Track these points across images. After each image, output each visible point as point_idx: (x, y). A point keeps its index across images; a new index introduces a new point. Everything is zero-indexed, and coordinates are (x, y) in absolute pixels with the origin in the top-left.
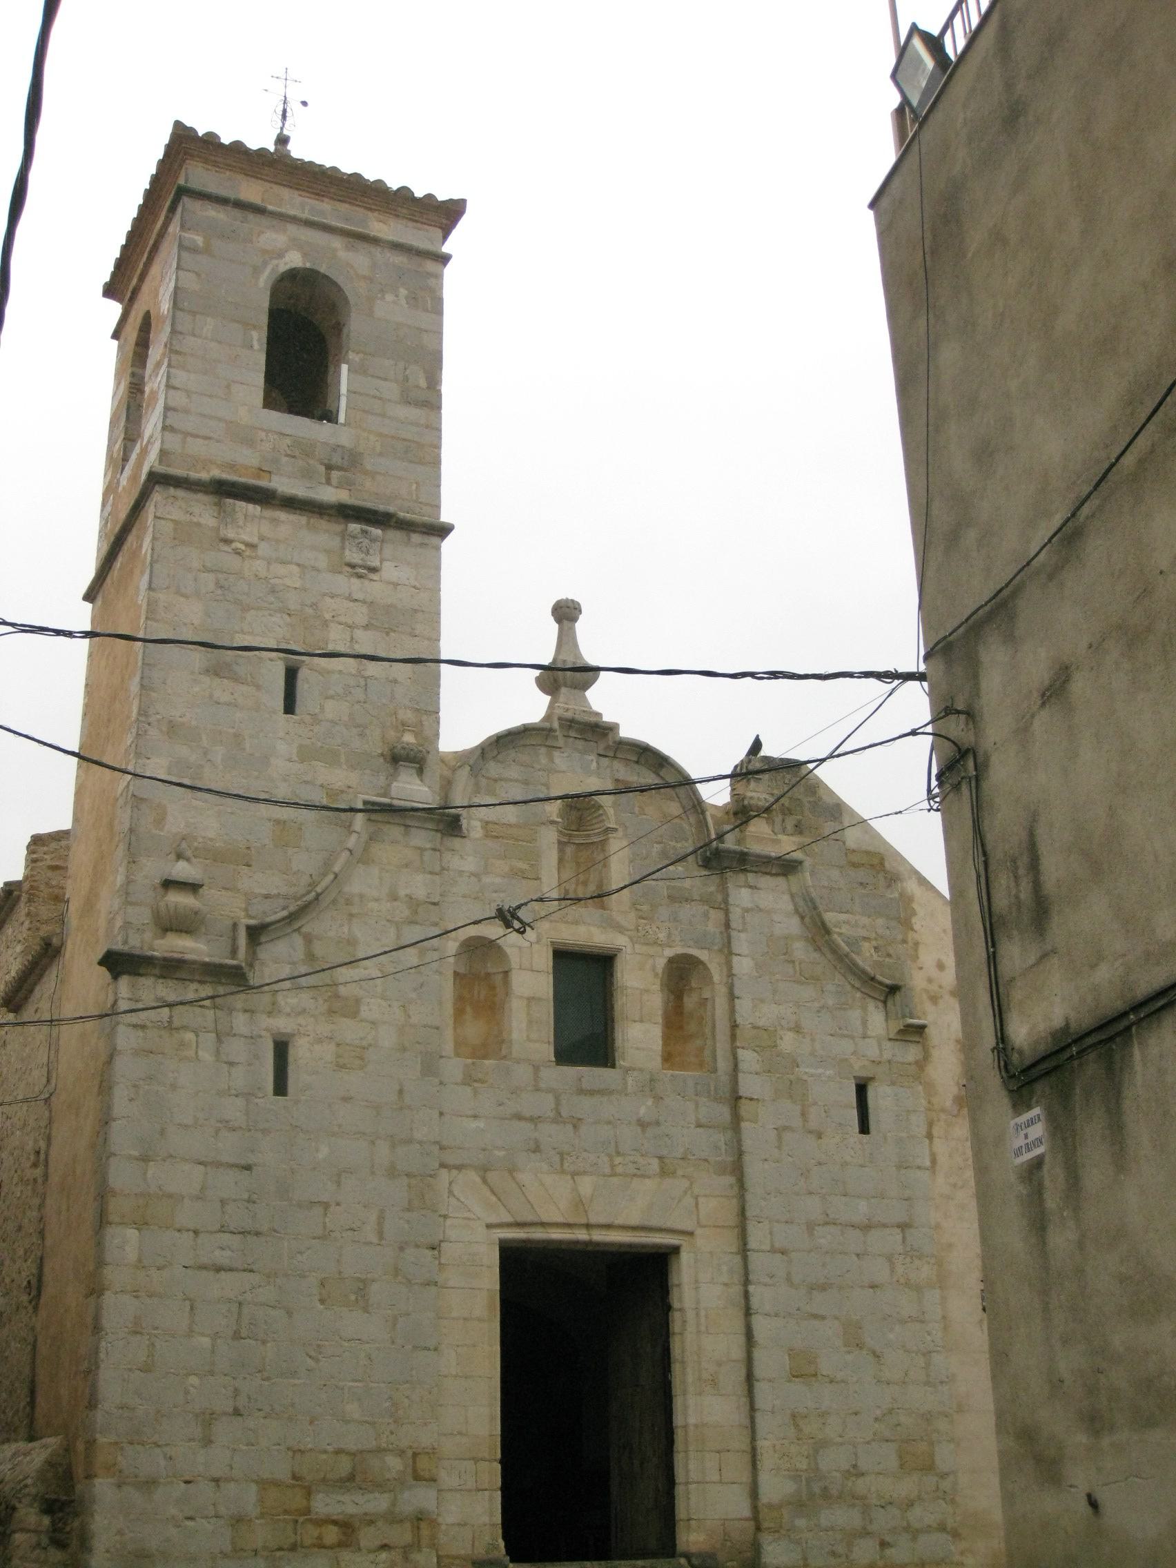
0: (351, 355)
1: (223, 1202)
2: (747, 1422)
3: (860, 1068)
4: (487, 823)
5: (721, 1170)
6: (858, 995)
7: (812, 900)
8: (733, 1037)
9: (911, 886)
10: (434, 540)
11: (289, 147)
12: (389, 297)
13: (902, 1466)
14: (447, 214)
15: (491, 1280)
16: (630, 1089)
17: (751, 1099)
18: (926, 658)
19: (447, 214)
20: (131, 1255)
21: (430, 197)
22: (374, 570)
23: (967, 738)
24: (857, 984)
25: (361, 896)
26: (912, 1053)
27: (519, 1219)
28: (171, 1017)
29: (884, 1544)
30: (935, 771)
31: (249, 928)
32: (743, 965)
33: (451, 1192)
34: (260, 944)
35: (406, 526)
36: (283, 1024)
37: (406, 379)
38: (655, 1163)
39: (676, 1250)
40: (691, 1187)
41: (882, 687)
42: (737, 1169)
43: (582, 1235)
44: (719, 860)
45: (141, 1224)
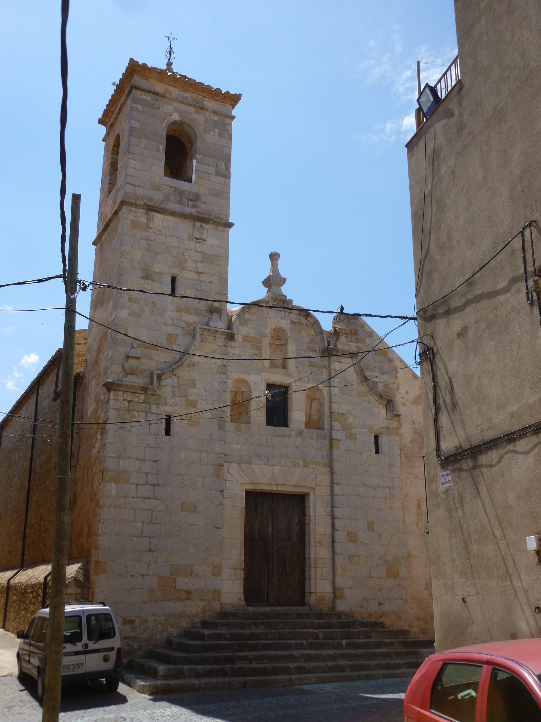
0: (197, 156)
1: (147, 474)
2: (332, 557)
4: (244, 336)
5: (325, 465)
6: (377, 403)
7: (361, 368)
8: (331, 417)
9: (397, 363)
10: (227, 229)
11: (172, 67)
12: (212, 133)
14: (235, 99)
15: (241, 504)
17: (337, 440)
18: (417, 313)
19: (235, 99)
20: (114, 493)
21: (228, 92)
22: (204, 240)
23: (430, 343)
24: (376, 398)
25: (198, 363)
26: (395, 424)
28: (129, 406)
29: (380, 604)
30: (418, 352)
31: (157, 374)
32: (335, 391)
33: (228, 471)
35: (218, 224)
36: (168, 409)
37: (217, 166)
39: (308, 494)
41: (402, 321)
42: (330, 465)
44: (329, 352)
45: (117, 481)
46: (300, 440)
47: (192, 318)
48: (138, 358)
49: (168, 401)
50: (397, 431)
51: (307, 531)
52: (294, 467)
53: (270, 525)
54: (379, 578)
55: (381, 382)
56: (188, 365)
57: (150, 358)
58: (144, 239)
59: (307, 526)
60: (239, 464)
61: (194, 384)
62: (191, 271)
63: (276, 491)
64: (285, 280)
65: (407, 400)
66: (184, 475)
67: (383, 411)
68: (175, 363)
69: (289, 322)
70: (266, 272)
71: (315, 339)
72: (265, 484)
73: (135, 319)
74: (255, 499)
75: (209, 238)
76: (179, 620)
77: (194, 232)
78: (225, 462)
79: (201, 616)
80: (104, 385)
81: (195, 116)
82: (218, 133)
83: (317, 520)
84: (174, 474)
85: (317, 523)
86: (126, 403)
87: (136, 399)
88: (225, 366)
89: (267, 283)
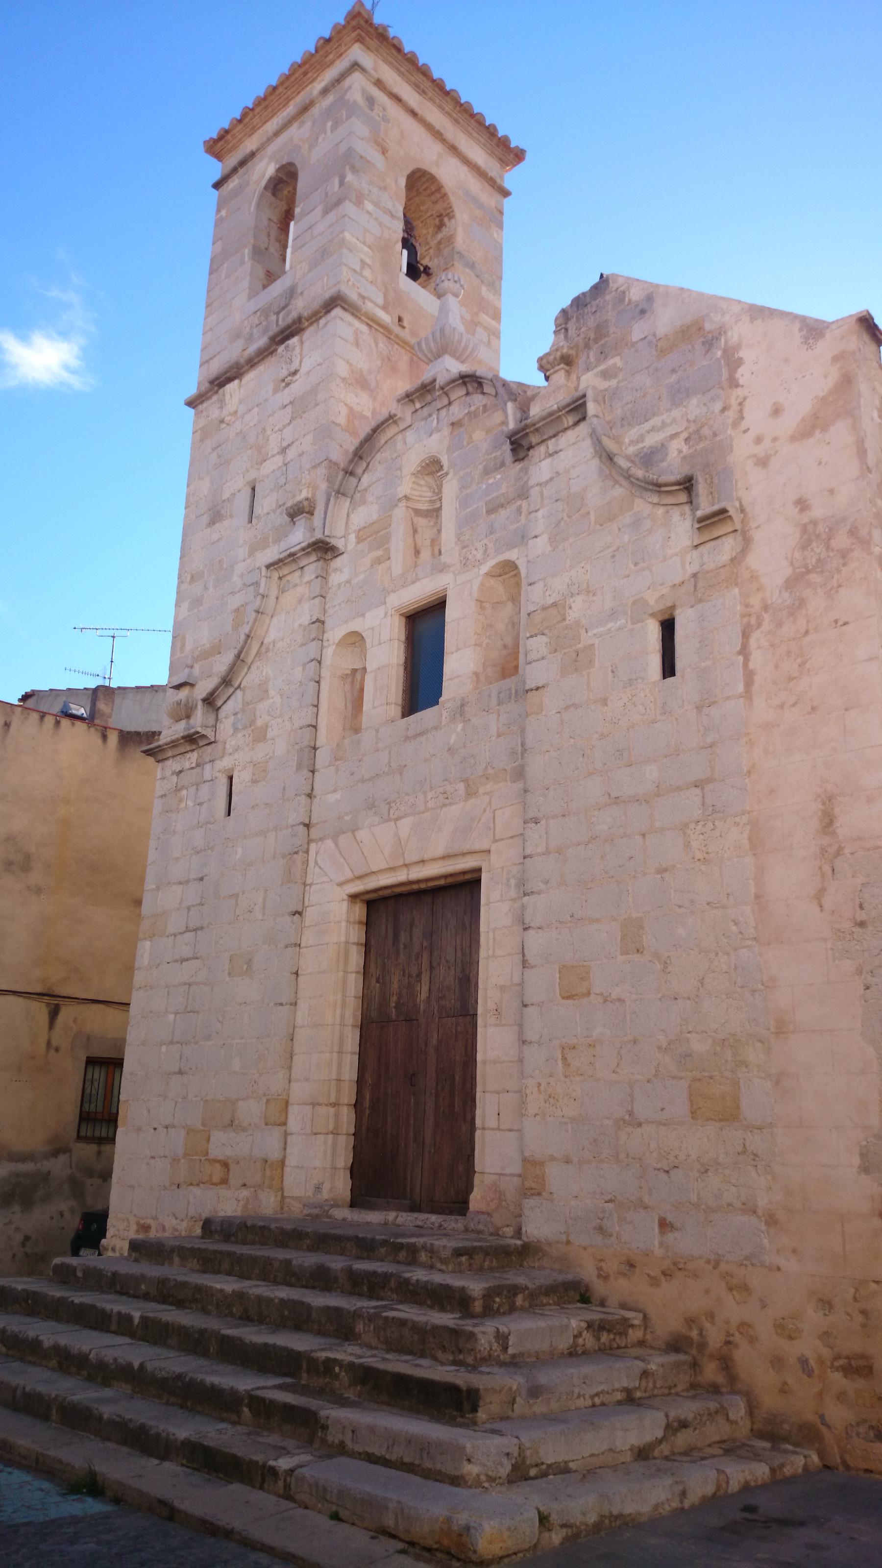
3: (654, 600)
6: (661, 511)
13: (693, 1113)
17: (537, 689)
27: (357, 874)
29: (664, 1225)
33: (316, 863)
34: (219, 708)
36: (226, 763)
38: (461, 787)
43: (402, 876)
46: (460, 727)
53: (425, 978)
54: (661, 1123)
72: (382, 871)
80: (606, 705)
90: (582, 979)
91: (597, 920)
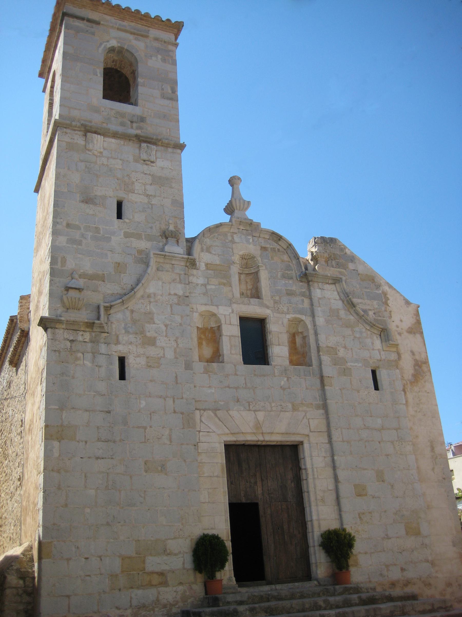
4: (207, 264)
5: (318, 407)
6: (369, 332)
12: (154, 58)
14: (177, 28)
15: (221, 459)
16: (276, 374)
22: (152, 162)
24: (368, 328)
25: (155, 294)
28: (71, 347)
29: (403, 570)
31: (105, 307)
32: (320, 321)
33: (201, 421)
35: (167, 146)
36: (121, 349)
37: (163, 89)
38: (290, 406)
39: (302, 443)
40: (305, 415)
42: (325, 407)
47: (143, 245)
48: (80, 290)
49: (120, 338)
50: (395, 364)
51: (304, 488)
52: (281, 411)
53: (259, 483)
54: (398, 537)
55: (370, 310)
56: (142, 297)
57: (95, 290)
58: (82, 161)
59: (305, 482)
60: (215, 410)
61: (152, 319)
62: (140, 194)
63: (262, 441)
64: (249, 203)
65: (402, 329)
66: (145, 428)
67: (378, 343)
68: (125, 295)
69: (259, 248)
70: (226, 196)
71: (290, 265)
73: (75, 246)
74: (236, 453)
75: (158, 159)
76: (152, 612)
77: (140, 154)
78: (197, 409)
79: (181, 604)
81: (134, 42)
82: (161, 59)
83: (315, 473)
84: (133, 427)
85: (316, 476)
86: (69, 344)
87: (80, 338)
88: (188, 297)
89: (229, 209)
90: (363, 490)
91: (366, 469)
